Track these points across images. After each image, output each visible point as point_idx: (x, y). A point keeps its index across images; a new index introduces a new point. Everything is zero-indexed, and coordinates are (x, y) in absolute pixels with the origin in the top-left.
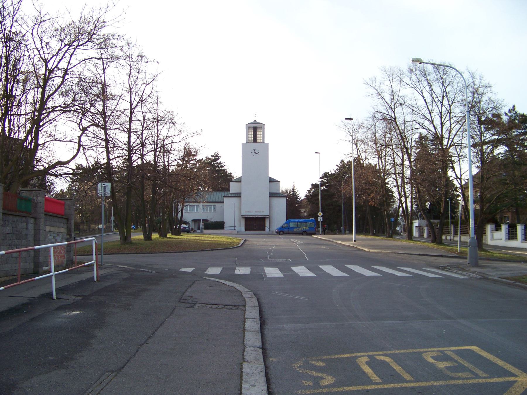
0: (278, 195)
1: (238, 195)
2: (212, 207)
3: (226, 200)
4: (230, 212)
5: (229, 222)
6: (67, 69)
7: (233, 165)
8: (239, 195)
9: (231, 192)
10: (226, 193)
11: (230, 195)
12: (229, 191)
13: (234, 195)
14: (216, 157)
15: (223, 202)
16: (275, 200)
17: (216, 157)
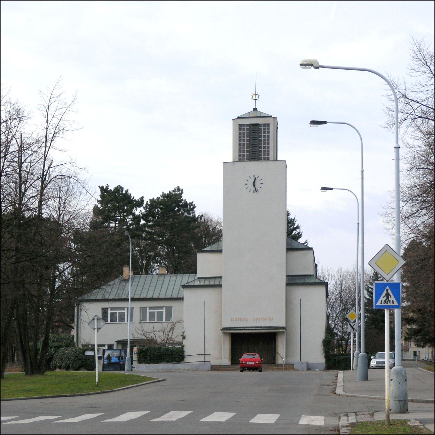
0: (308, 281)
1: (214, 283)
2: (164, 310)
3: (187, 294)
4: (200, 322)
5: (192, 349)
6: (420, 117)
7: (207, 201)
8: (217, 283)
9: (199, 275)
10: (186, 279)
11: (197, 283)
12: (195, 272)
13: (207, 283)
14: (104, 190)
15: (182, 299)
16: (301, 293)
17: (104, 190)
